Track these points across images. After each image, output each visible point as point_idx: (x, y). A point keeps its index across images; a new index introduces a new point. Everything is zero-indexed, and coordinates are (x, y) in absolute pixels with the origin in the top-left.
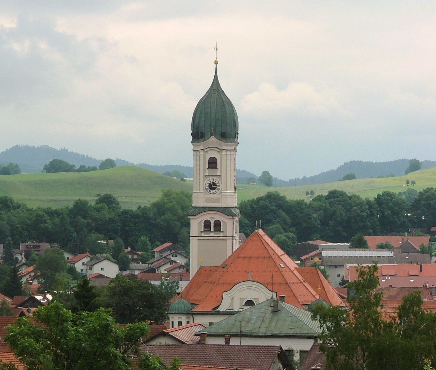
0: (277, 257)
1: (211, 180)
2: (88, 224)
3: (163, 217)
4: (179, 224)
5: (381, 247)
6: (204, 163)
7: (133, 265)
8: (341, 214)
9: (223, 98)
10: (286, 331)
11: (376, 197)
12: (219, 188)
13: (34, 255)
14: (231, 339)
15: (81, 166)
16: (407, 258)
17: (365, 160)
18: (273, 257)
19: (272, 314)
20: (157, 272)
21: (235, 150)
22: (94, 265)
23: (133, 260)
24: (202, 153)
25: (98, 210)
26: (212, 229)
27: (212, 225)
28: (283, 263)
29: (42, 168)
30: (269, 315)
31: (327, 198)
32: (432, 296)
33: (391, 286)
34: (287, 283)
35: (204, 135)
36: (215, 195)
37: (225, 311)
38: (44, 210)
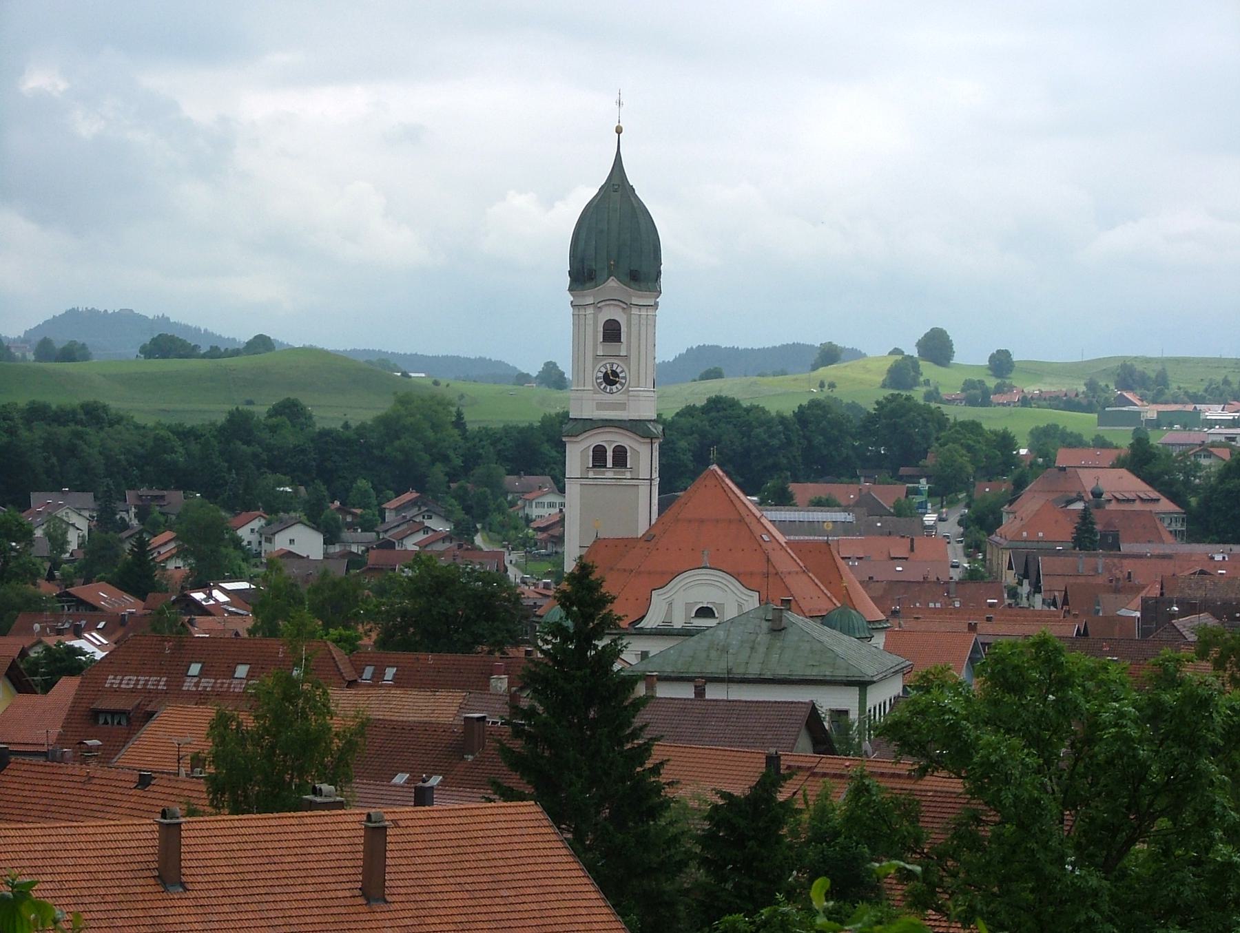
0: (755, 521)
1: (608, 365)
2: (255, 455)
3: (397, 443)
4: (427, 458)
5: (819, 504)
6: (595, 331)
7: (346, 535)
8: (732, 442)
9: (634, 202)
10: (800, 671)
11: (796, 410)
12: (624, 381)
13: (156, 514)
14: (706, 687)
15: (211, 347)
16: (879, 524)
17: (725, 343)
18: (747, 520)
19: (769, 636)
20: (397, 548)
21: (656, 306)
22: (275, 533)
23: (351, 526)
24: (590, 311)
25: (273, 429)
26: (609, 463)
27: (610, 454)
28: (766, 532)
29: (136, 351)
30: (763, 638)
31: (706, 410)
32: (950, 598)
33: (871, 578)
34: (777, 574)
35: (595, 277)
36: (616, 395)
37: (655, 628)
38: (169, 428)
